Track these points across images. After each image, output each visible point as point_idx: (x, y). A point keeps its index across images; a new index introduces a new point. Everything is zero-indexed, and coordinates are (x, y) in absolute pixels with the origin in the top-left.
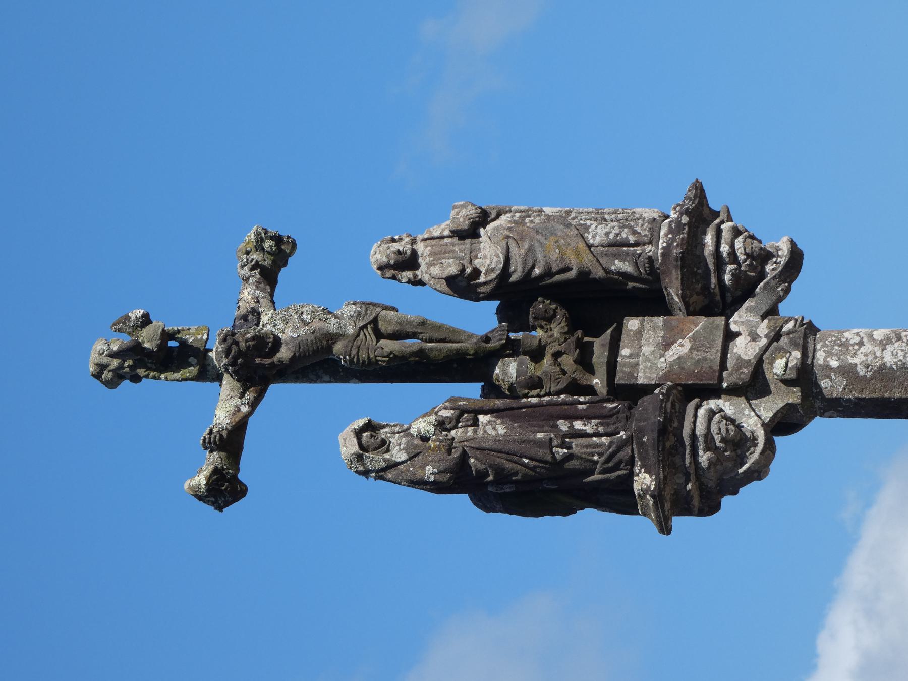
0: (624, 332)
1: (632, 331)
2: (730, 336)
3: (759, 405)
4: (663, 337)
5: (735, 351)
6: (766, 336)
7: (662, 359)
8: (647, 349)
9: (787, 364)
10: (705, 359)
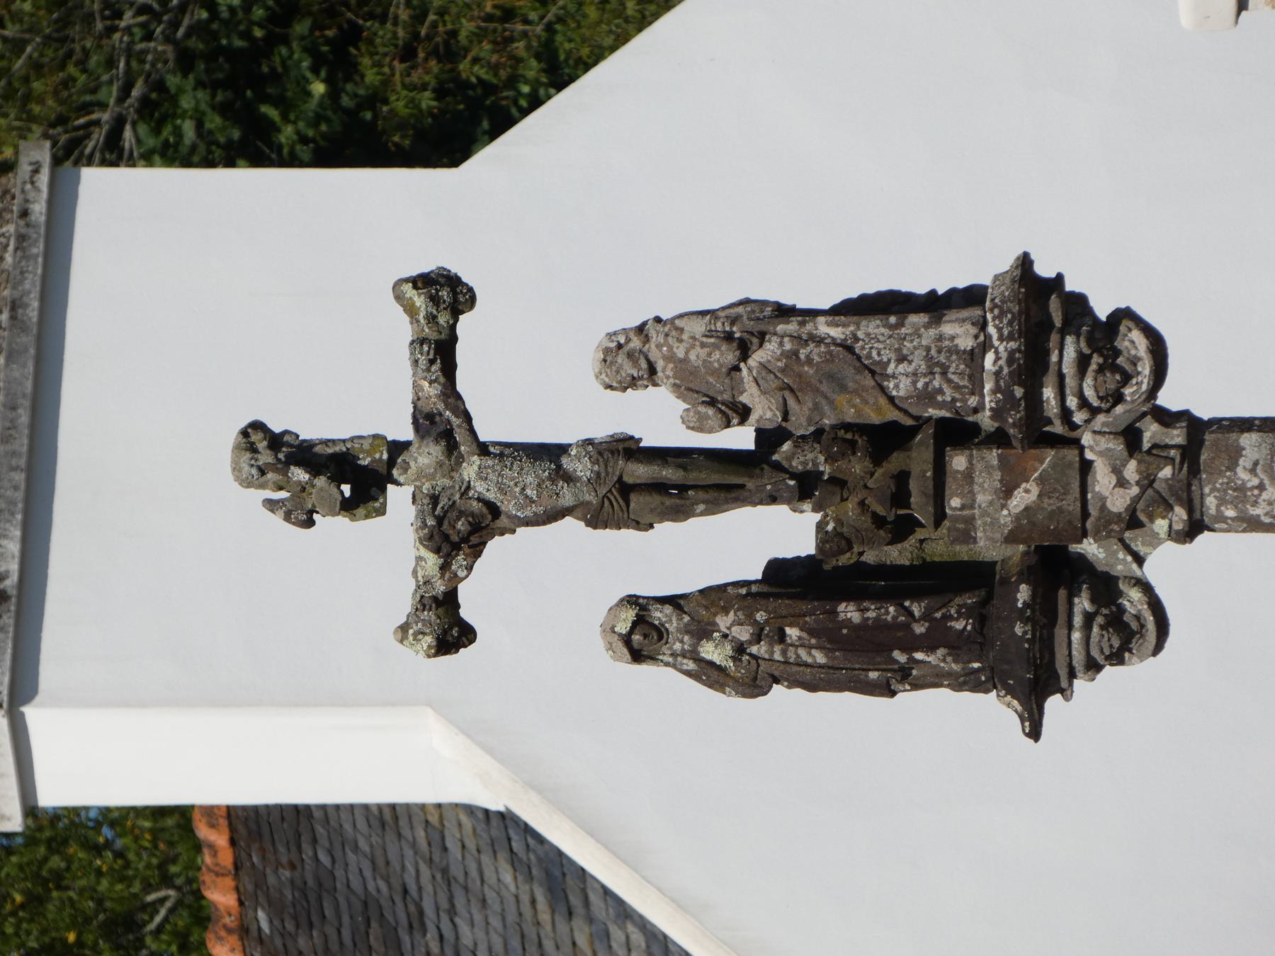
0: (948, 474)
1: (958, 471)
2: (1086, 467)
3: (1135, 539)
4: (1001, 481)
5: (1097, 489)
6: (1138, 483)
7: (1005, 512)
8: (982, 498)
9: (1170, 526)
10: (1060, 510)
